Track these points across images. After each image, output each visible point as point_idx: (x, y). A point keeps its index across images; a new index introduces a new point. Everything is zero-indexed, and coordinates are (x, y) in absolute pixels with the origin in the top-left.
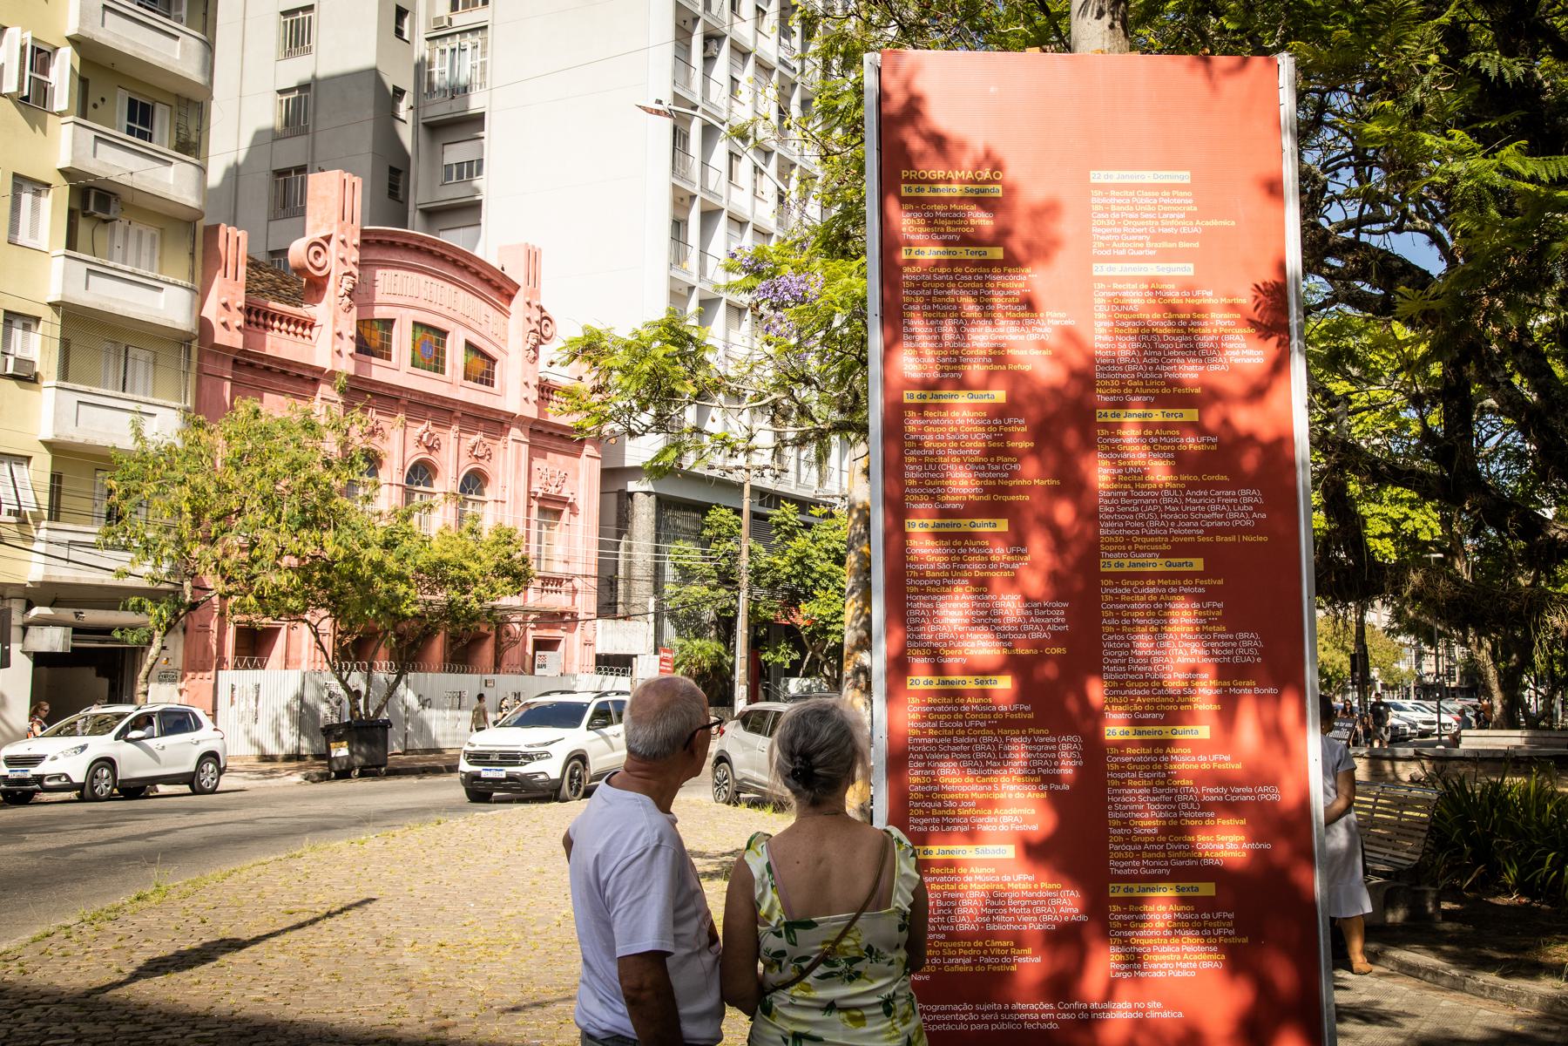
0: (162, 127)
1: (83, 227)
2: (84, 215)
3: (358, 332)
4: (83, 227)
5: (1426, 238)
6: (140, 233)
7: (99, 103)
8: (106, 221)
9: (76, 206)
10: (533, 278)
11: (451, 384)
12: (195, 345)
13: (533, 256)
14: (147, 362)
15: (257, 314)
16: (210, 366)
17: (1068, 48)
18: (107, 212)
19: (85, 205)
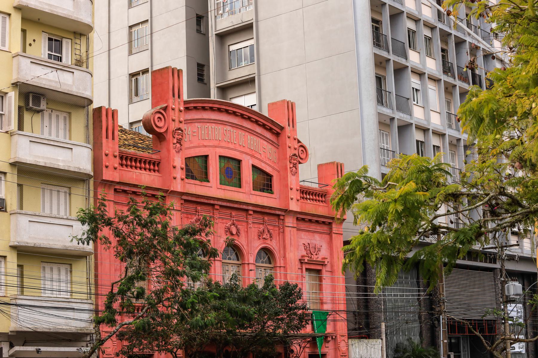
0: (67, 49)
1: (27, 117)
2: (27, 110)
3: (186, 165)
4: (27, 117)
5: (295, 230)
6: (57, 116)
7: (32, 43)
8: (38, 112)
9: (22, 104)
10: (292, 121)
11: (247, 194)
12: (92, 181)
13: (290, 107)
14: (65, 192)
15: (126, 159)
16: (101, 191)
17: (240, 186)
18: (39, 106)
19: (27, 103)
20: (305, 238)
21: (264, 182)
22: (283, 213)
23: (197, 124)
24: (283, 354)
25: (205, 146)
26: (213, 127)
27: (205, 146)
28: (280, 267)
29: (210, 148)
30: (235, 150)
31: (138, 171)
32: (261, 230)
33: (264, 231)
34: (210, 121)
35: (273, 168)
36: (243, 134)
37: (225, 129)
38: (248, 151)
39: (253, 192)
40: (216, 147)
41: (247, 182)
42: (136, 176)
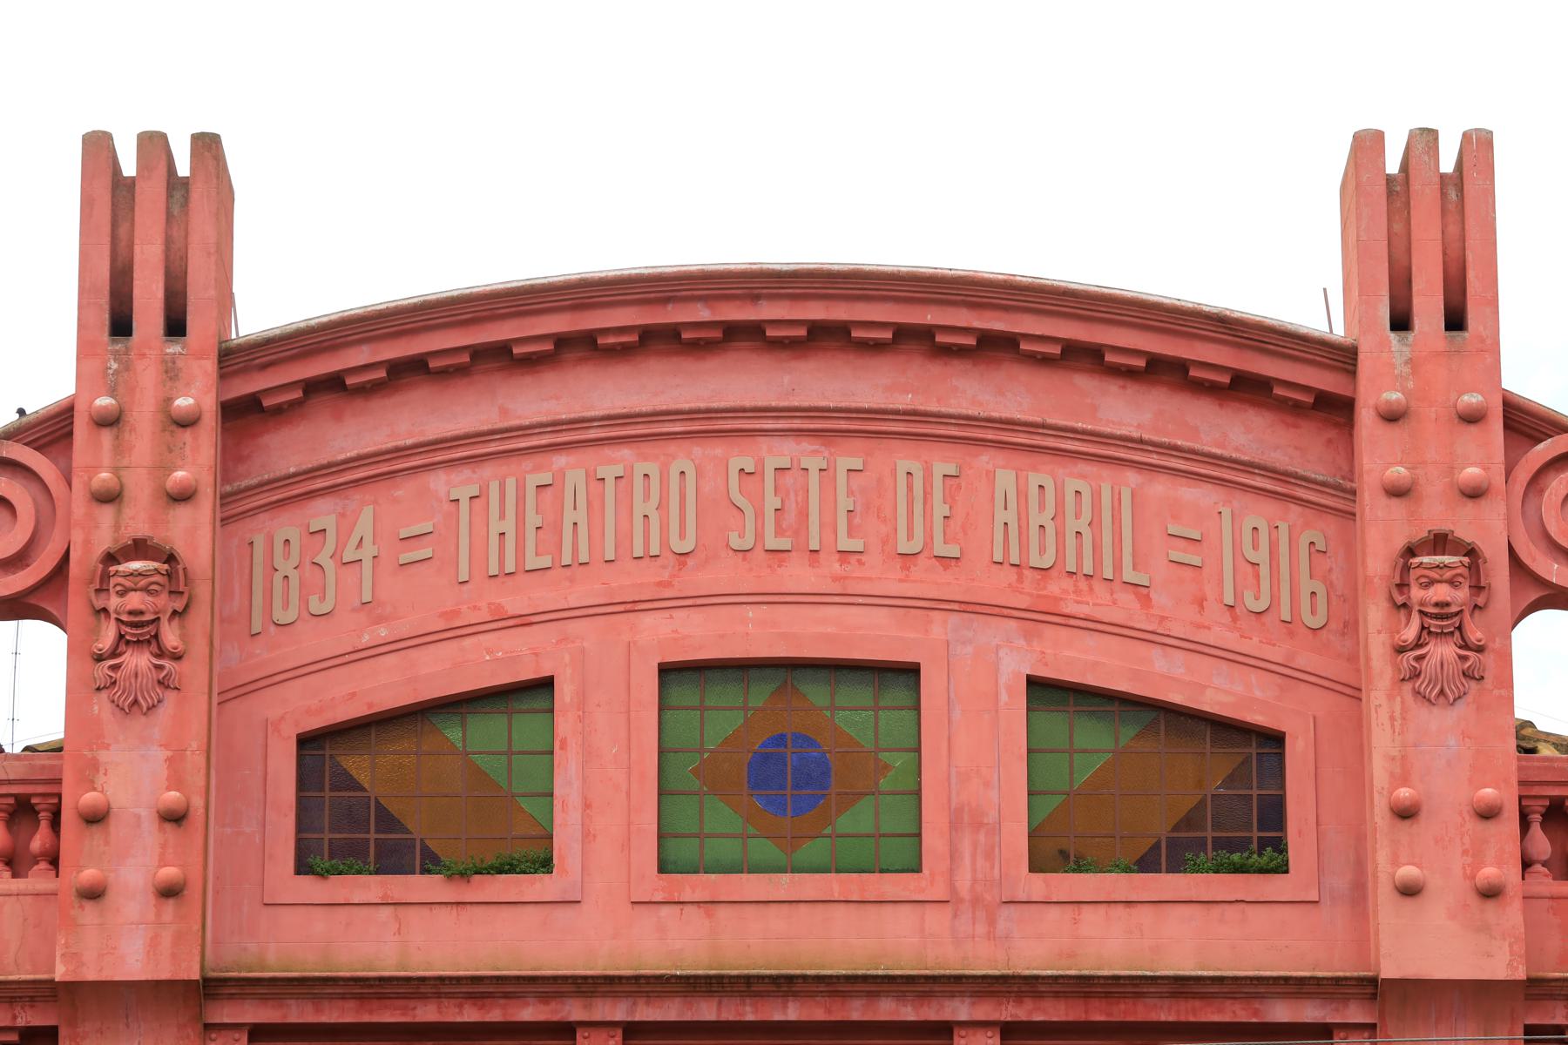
23: (439, 482)
25: (524, 621)
26: (609, 472)
27: (524, 621)
29: (574, 627)
30: (847, 599)
33: (965, 533)
34: (571, 435)
35: (1289, 675)
36: (941, 468)
37: (736, 463)
39: (1038, 885)
40: (632, 607)
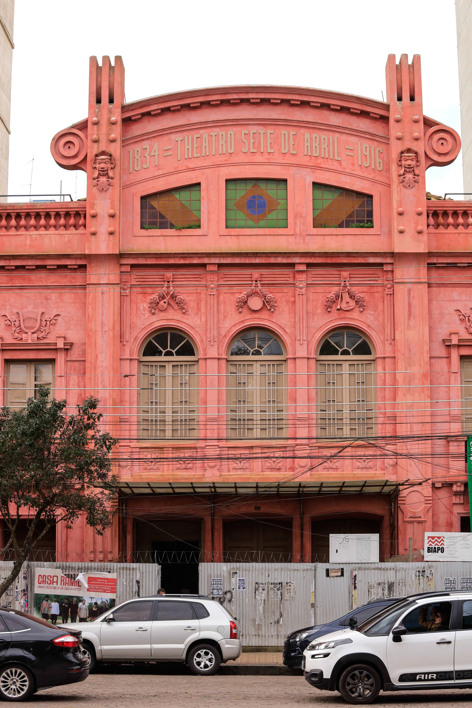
20: (464, 298)
21: (356, 209)
22: (389, 260)
23: (173, 137)
24: (387, 518)
25: (193, 169)
26: (213, 134)
27: (193, 169)
28: (131, 360)
30: (269, 164)
31: (33, 232)
32: (332, 295)
35: (374, 181)
36: (292, 133)
37: (243, 132)
38: (305, 161)
39: (315, 231)
41: (297, 215)
42: (31, 240)
